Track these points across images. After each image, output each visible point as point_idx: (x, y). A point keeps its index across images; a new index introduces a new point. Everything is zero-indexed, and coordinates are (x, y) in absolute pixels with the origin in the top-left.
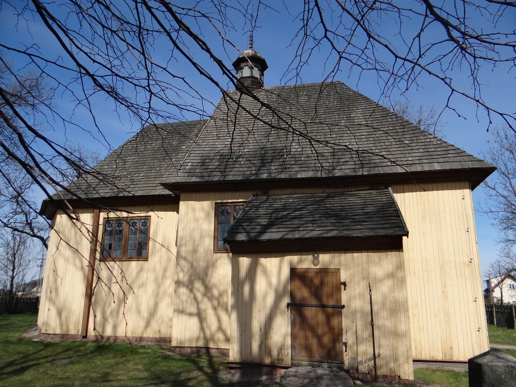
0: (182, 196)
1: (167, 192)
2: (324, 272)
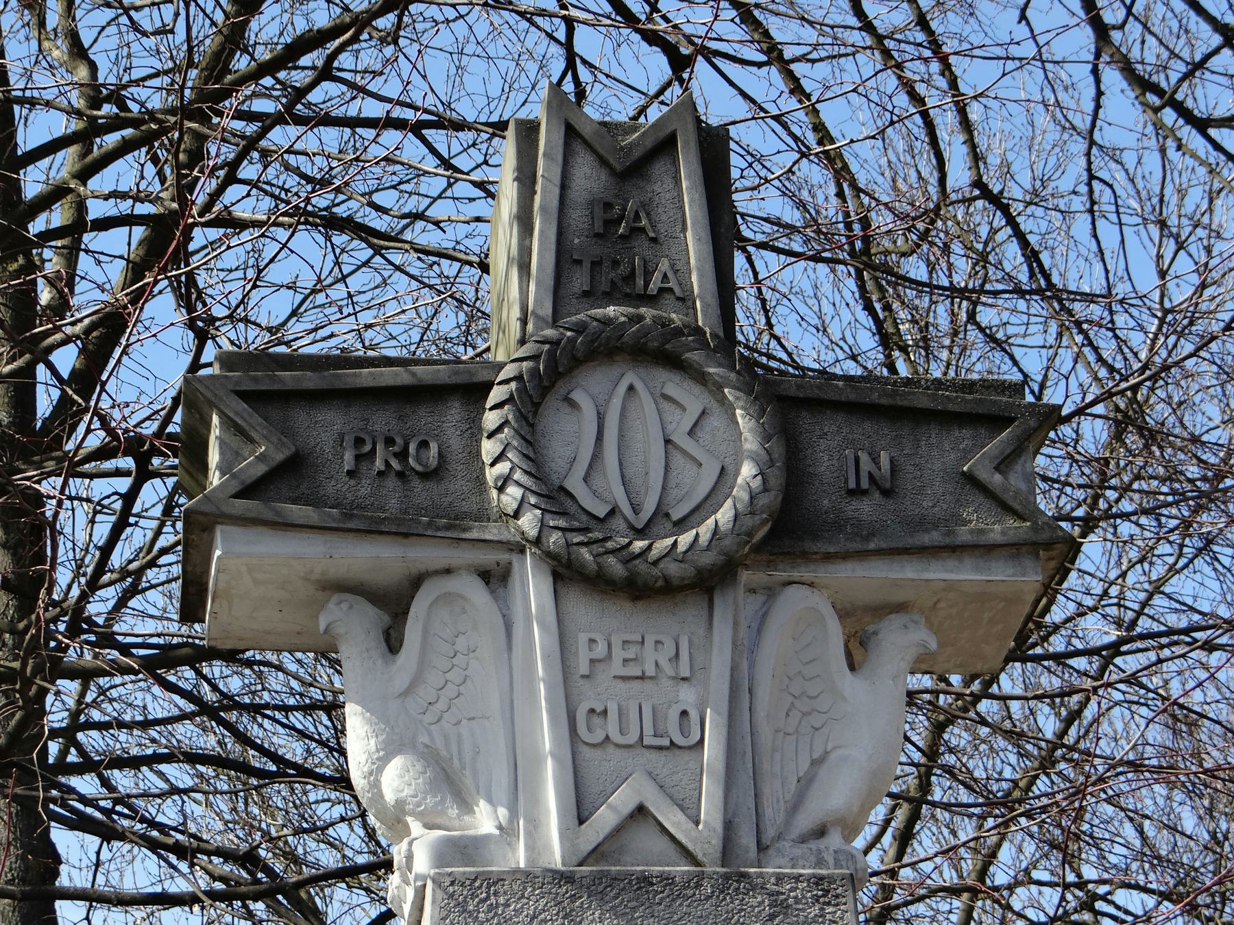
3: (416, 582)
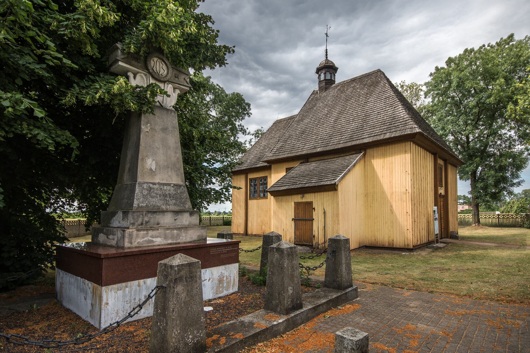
0: (272, 166)
1: (266, 164)
2: (311, 203)
3: (138, 73)
